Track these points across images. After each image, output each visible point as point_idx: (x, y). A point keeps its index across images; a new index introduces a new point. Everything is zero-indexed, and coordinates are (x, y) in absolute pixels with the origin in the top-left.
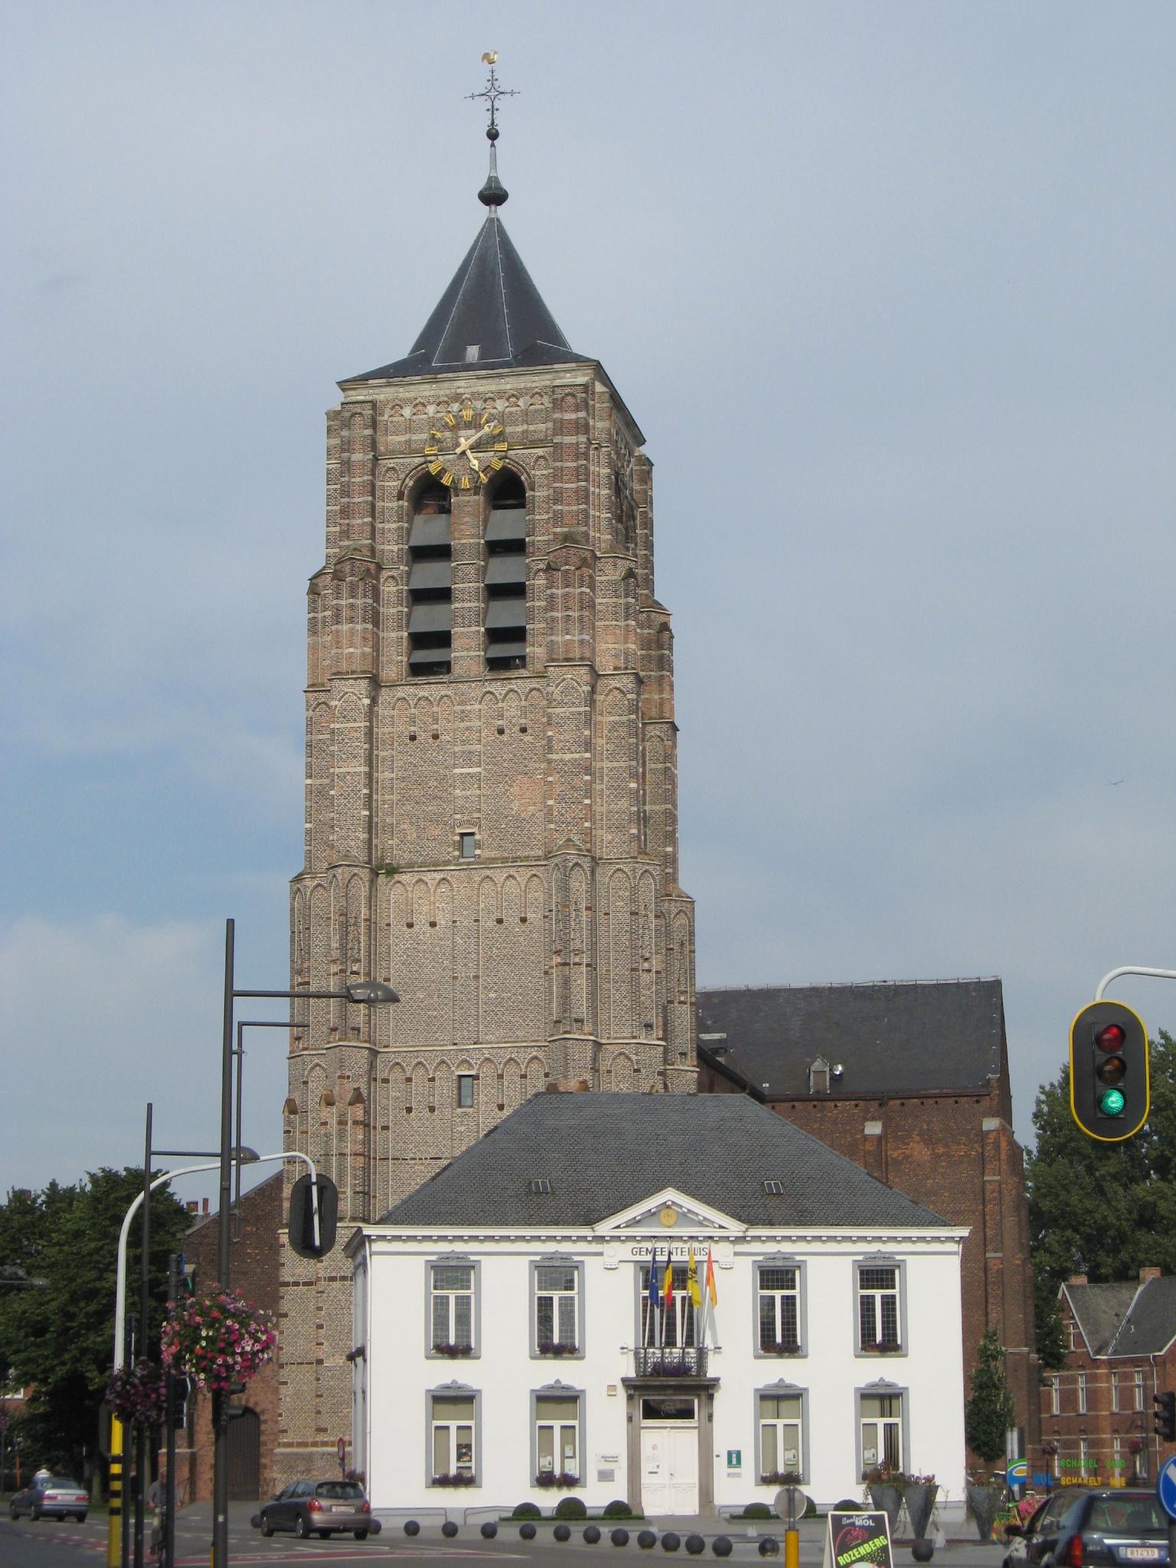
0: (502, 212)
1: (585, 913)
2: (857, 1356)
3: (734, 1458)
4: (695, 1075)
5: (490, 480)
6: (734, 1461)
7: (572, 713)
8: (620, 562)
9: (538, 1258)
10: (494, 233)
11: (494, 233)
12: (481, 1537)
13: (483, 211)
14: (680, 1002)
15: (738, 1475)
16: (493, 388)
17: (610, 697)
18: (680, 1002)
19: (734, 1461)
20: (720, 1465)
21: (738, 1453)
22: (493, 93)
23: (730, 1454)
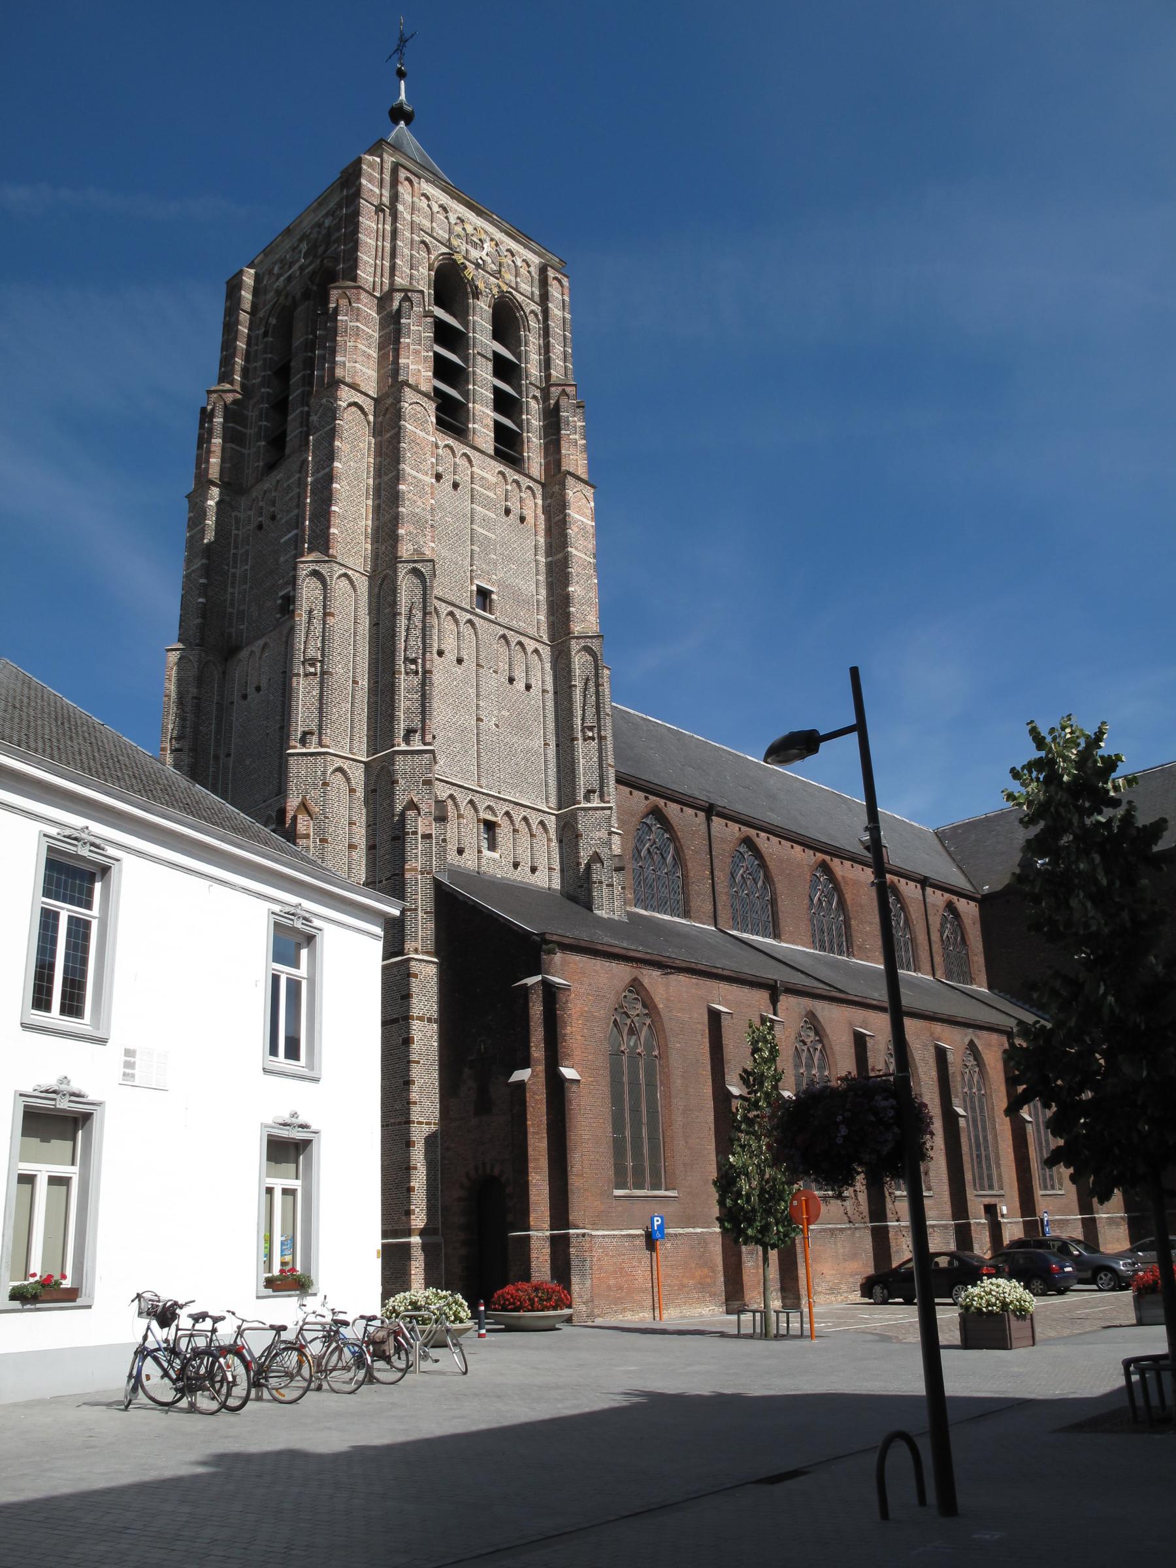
16: (324, 212)
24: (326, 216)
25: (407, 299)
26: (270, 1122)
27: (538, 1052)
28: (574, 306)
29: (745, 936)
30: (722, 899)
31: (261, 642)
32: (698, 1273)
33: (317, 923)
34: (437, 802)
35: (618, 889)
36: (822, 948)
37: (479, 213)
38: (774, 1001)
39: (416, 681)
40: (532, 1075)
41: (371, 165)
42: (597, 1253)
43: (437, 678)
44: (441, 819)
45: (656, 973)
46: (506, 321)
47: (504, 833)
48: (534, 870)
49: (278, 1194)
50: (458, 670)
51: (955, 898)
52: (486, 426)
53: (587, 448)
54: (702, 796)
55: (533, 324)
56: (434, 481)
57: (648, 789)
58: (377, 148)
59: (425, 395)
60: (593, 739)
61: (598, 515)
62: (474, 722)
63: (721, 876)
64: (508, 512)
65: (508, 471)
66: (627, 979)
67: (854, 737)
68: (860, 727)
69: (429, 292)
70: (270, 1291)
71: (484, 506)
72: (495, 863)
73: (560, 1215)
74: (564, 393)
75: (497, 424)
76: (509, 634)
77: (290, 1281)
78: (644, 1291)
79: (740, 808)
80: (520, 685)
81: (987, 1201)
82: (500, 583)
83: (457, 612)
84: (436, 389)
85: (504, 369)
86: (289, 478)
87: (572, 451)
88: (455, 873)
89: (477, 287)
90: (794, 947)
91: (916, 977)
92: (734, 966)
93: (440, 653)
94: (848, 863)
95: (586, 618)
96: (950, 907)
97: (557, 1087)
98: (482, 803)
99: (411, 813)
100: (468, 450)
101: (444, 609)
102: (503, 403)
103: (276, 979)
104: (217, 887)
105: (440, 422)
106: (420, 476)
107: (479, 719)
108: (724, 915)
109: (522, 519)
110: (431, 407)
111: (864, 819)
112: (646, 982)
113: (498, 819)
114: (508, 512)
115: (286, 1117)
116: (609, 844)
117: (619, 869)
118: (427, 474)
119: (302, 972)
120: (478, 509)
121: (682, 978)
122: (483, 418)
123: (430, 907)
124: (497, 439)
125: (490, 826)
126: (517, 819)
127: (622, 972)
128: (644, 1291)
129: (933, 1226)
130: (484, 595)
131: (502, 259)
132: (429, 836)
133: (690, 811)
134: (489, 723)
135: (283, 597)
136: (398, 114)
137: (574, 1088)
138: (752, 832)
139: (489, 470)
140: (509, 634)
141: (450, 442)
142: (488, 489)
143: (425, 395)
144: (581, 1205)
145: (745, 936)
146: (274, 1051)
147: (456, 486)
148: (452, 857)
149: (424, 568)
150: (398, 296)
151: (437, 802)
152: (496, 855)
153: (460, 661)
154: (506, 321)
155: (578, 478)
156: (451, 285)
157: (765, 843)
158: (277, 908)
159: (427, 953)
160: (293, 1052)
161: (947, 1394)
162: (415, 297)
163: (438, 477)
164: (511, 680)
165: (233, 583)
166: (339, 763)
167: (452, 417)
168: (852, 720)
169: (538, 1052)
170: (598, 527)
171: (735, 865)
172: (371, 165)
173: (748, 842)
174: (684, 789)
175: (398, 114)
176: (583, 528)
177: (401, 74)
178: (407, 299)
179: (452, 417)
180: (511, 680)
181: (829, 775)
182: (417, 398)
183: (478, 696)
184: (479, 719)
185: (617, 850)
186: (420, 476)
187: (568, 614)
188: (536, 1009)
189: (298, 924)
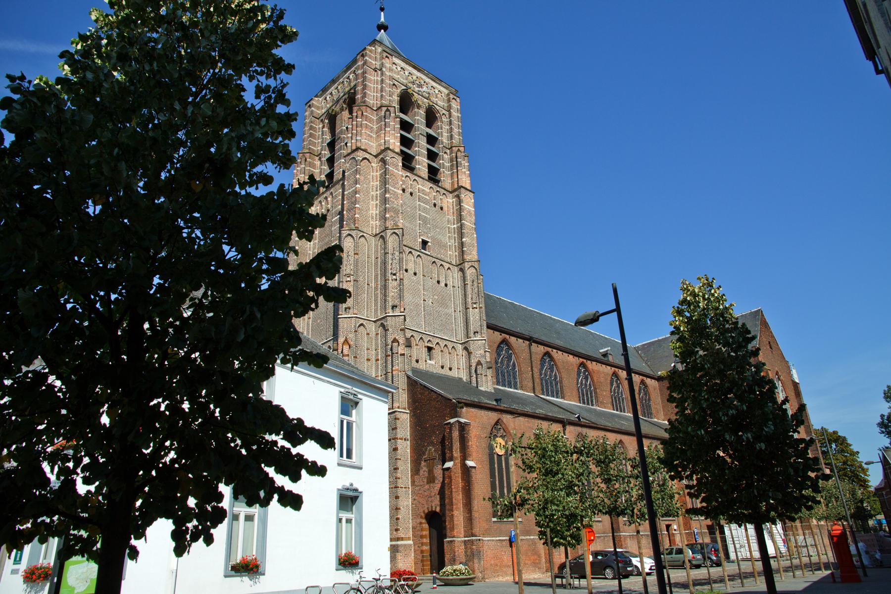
25: (388, 110)
26: (340, 487)
27: (457, 453)
28: (461, 111)
29: (548, 398)
30: (537, 381)
32: (532, 558)
33: (360, 396)
34: (407, 339)
35: (489, 378)
36: (584, 403)
37: (419, 70)
38: (564, 426)
39: (395, 283)
40: (454, 465)
41: (371, 51)
42: (486, 548)
43: (406, 282)
44: (409, 346)
45: (509, 417)
46: (431, 117)
48: (450, 369)
49: (344, 521)
50: (414, 278)
51: (645, 378)
53: (470, 175)
54: (526, 333)
55: (444, 119)
57: (502, 331)
58: (374, 42)
59: (397, 153)
61: (476, 205)
63: (536, 370)
64: (435, 205)
65: (434, 187)
66: (496, 419)
67: (615, 313)
68: (618, 310)
69: (397, 106)
70: (233, 573)
72: (431, 365)
73: (470, 530)
74: (459, 150)
75: (429, 165)
76: (437, 261)
77: (349, 562)
78: (508, 566)
79: (543, 338)
80: (443, 284)
81: (667, 523)
82: (432, 238)
83: (413, 251)
84: (401, 150)
85: (432, 140)
87: (463, 176)
88: (415, 371)
90: (571, 402)
92: (618, 427)
93: (406, 271)
94: (594, 363)
95: (472, 254)
96: (642, 382)
97: (467, 472)
98: (426, 339)
99: (395, 344)
100: (416, 178)
101: (407, 250)
102: (432, 156)
103: (342, 422)
104: (316, 381)
105: (404, 165)
108: (538, 388)
109: (442, 208)
110: (400, 159)
111: (621, 351)
112: (504, 420)
114: (435, 205)
115: (348, 485)
116: (485, 356)
117: (489, 368)
119: (354, 418)
121: (521, 419)
122: (422, 163)
123: (406, 387)
124: (429, 172)
125: (430, 349)
127: (493, 416)
128: (508, 566)
129: (409, 539)
130: (424, 243)
131: (432, 92)
132: (403, 355)
133: (520, 341)
136: (381, 27)
137: (473, 470)
138: (550, 349)
139: (427, 186)
140: (437, 261)
141: (408, 174)
143: (397, 153)
144: (480, 525)
145: (548, 398)
146: (342, 456)
147: (411, 194)
148: (414, 364)
149: (399, 232)
150: (384, 109)
151: (407, 339)
152: (433, 362)
153: (415, 274)
154: (431, 117)
155: (466, 189)
156: (406, 102)
157: (554, 353)
158: (343, 390)
159: (405, 409)
160: (349, 456)
161: (778, 589)
162: (392, 109)
163: (404, 190)
166: (361, 321)
167: (408, 162)
168: (614, 307)
169: (457, 453)
170: (475, 211)
171: (542, 365)
172: (371, 51)
173: (547, 354)
174: (518, 330)
175: (381, 27)
176: (469, 212)
177: (382, 9)
178: (388, 110)
179: (408, 162)
180: (438, 282)
181: (606, 329)
182: (393, 155)
185: (488, 360)
188: (456, 434)
189: (351, 397)
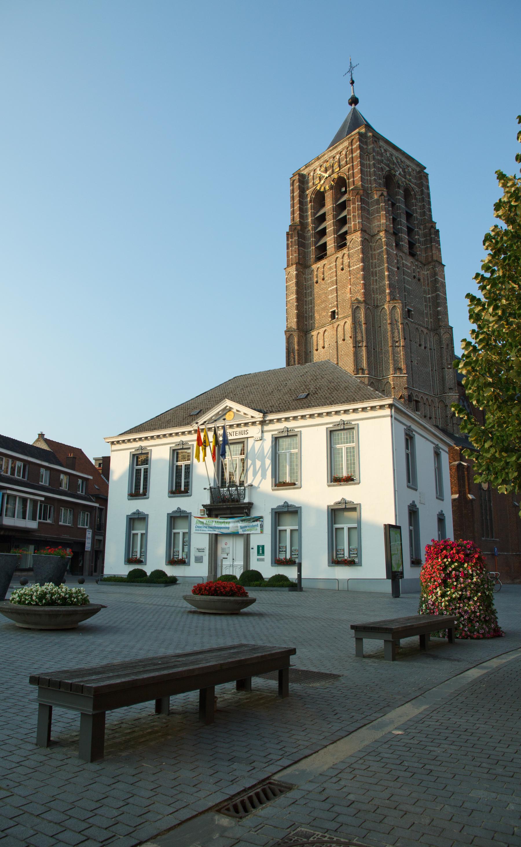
0: (358, 107)
1: (363, 325)
2: (329, 486)
3: (261, 550)
4: (458, 397)
5: (336, 183)
6: (261, 552)
7: (356, 251)
8: (378, 192)
9: (174, 445)
10: (355, 112)
11: (355, 112)
12: (191, 594)
13: (350, 108)
14: (448, 368)
15: (263, 560)
16: (336, 152)
17: (377, 243)
18: (448, 368)
19: (261, 552)
20: (253, 554)
21: (263, 547)
22: (352, 68)
23: (258, 547)
24: (337, 153)
31: (324, 329)
47: (421, 404)
52: (405, 243)
56: (396, 269)
60: (450, 368)
62: (410, 363)
71: (407, 276)
80: (423, 347)
86: (330, 264)
89: (399, 184)
91: (165, 607)
106: (392, 268)
107: (412, 362)
113: (419, 400)
114: (414, 277)
118: (394, 267)
120: (406, 277)
126: (425, 399)
134: (415, 363)
135: (331, 312)
142: (408, 269)
164: (420, 345)
165: (306, 304)
180: (420, 345)
183: (411, 352)
184: (412, 362)
186: (392, 268)
187: (365, 289)
